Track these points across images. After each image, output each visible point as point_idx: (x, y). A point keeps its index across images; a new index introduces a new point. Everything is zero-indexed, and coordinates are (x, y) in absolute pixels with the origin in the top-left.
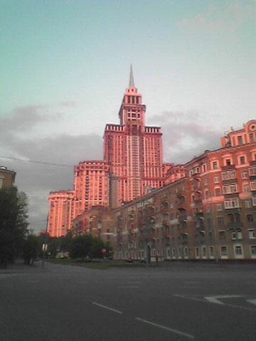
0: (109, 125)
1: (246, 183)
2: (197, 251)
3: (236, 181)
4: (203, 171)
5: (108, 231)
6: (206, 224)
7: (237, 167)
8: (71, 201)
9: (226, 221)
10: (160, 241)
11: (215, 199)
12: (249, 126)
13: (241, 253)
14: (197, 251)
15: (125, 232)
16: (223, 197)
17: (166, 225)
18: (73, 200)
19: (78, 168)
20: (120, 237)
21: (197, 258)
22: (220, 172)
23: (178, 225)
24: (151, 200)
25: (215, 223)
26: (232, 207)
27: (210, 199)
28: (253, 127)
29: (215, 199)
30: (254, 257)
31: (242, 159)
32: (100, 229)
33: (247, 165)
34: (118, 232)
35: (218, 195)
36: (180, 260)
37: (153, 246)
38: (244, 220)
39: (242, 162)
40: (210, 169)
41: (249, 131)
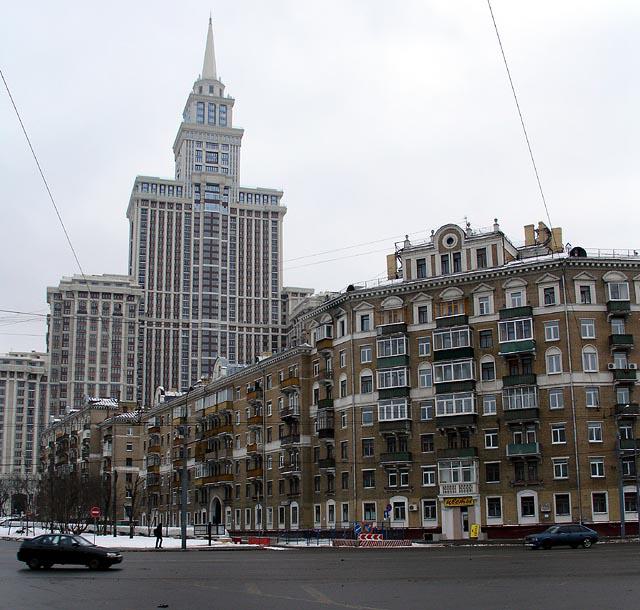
0: (142, 183)
1: (425, 366)
2: (318, 512)
3: (407, 360)
4: (339, 335)
5: (129, 462)
6: (337, 454)
7: (411, 329)
8: (38, 381)
9: (380, 447)
10: (243, 490)
11: (361, 399)
12: (440, 243)
13: (603, 509)
14: (318, 512)
15: (166, 469)
16: (376, 395)
17: (258, 459)
18: (44, 378)
19: (58, 295)
20: (154, 478)
21: (317, 526)
22: (373, 340)
23: (247, 461)
24: (224, 396)
25: (353, 453)
26: (393, 419)
27: (349, 399)
28: (450, 241)
29: (361, 399)
30: (631, 517)
31: (422, 311)
32: (108, 459)
33: (431, 325)
34: (150, 469)
35: (365, 391)
36: (282, 532)
37: (228, 501)
38: (415, 446)
39: (423, 320)
40: (571, 300)
41: (441, 248)
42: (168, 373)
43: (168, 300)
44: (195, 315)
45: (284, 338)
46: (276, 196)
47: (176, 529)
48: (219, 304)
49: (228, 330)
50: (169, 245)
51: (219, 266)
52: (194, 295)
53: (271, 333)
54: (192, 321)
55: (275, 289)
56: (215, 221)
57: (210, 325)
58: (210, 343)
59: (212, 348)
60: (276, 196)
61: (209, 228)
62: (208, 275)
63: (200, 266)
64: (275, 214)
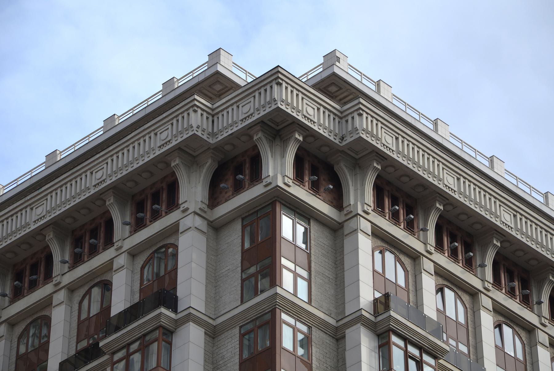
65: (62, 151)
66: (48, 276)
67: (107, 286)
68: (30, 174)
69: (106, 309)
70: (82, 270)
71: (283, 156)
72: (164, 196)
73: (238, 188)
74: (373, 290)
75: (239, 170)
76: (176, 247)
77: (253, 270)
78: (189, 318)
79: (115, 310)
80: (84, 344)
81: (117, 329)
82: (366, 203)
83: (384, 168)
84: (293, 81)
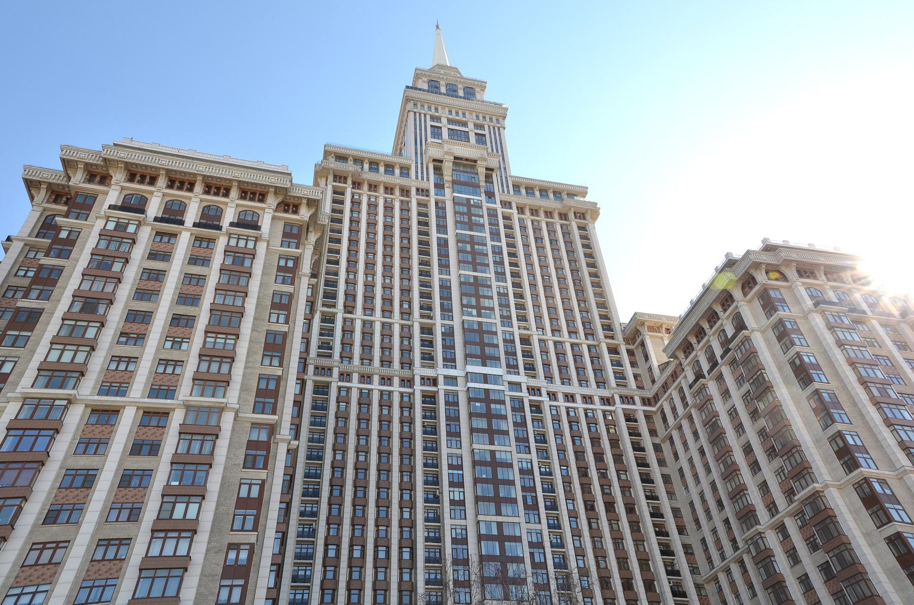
42: (346, 434)
43: (367, 334)
44: (450, 361)
45: (648, 417)
46: (587, 188)
47: (217, 346)
48: (523, 550)
49: (524, 394)
50: (408, 454)
51: (507, 450)
52: (447, 393)
53: (619, 407)
54: (441, 371)
55: (608, 328)
56: (501, 473)
57: (485, 378)
58: (495, 482)
59: (486, 341)
60: (587, 188)
61: (488, 489)
62: (486, 472)
63: (457, 324)
64: (580, 215)
65: (95, 336)
66: (705, 334)
67: (724, 331)
68: (33, 468)
69: (726, 336)
70: (714, 329)
71: (761, 274)
72: (729, 300)
73: (751, 288)
74: (223, 256)
75: (749, 283)
76: (739, 312)
77: (767, 310)
78: (753, 331)
79: (729, 337)
80: (724, 349)
81: (732, 341)
82: (180, 483)
83: (797, 264)
84: (755, 252)
